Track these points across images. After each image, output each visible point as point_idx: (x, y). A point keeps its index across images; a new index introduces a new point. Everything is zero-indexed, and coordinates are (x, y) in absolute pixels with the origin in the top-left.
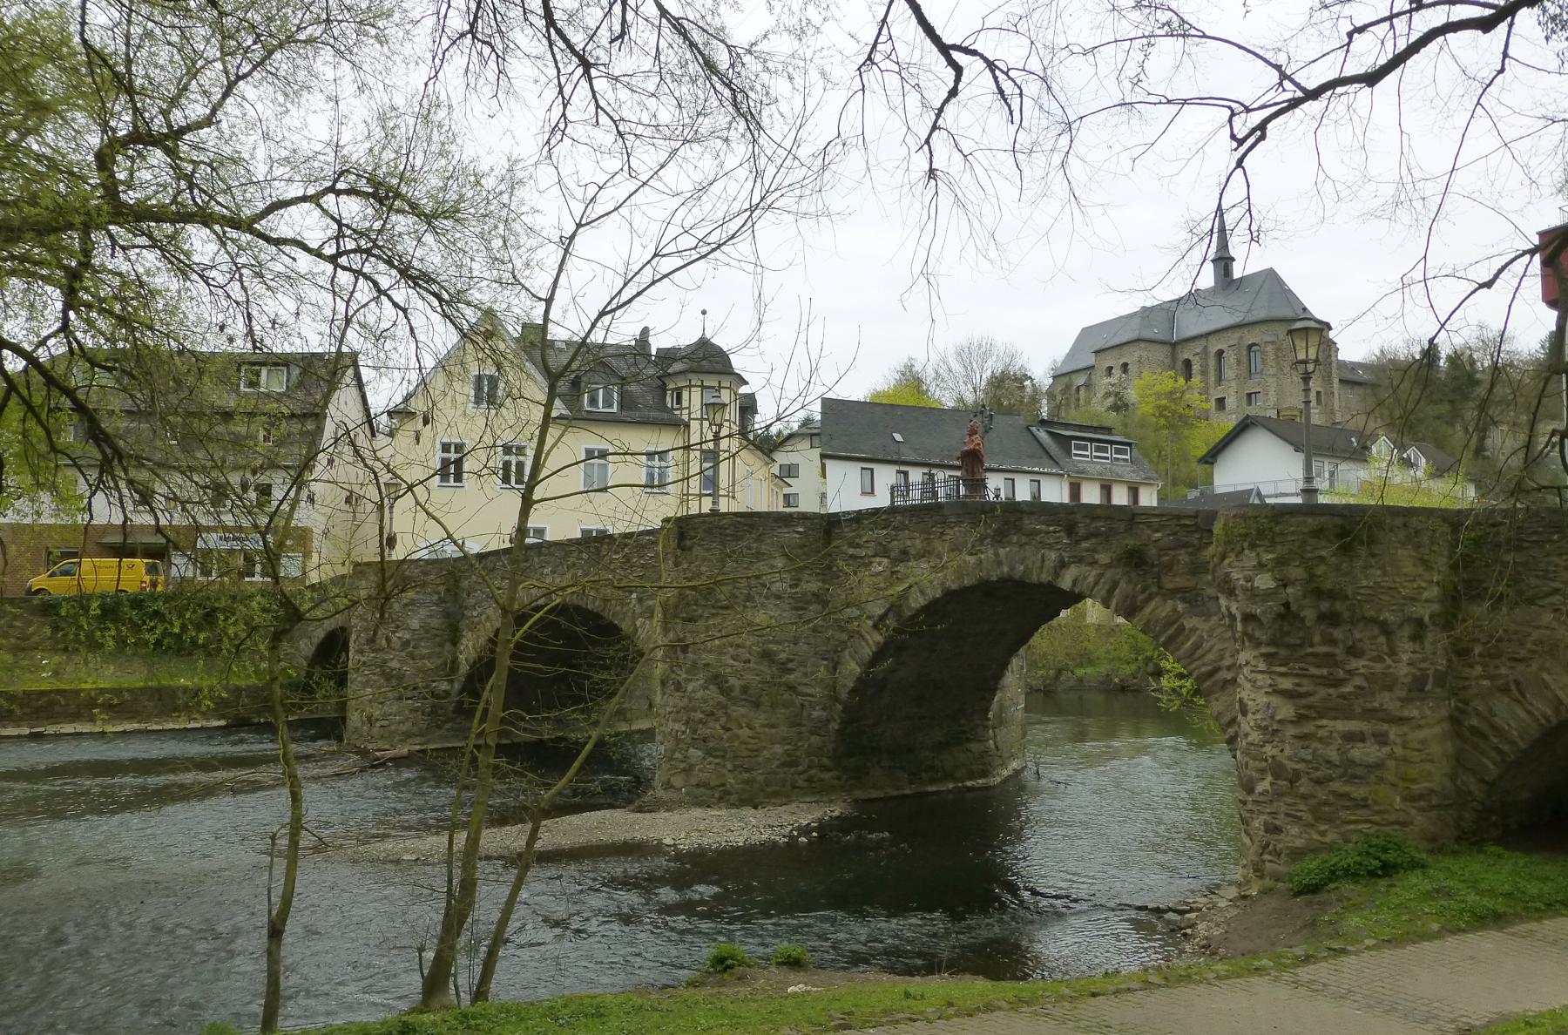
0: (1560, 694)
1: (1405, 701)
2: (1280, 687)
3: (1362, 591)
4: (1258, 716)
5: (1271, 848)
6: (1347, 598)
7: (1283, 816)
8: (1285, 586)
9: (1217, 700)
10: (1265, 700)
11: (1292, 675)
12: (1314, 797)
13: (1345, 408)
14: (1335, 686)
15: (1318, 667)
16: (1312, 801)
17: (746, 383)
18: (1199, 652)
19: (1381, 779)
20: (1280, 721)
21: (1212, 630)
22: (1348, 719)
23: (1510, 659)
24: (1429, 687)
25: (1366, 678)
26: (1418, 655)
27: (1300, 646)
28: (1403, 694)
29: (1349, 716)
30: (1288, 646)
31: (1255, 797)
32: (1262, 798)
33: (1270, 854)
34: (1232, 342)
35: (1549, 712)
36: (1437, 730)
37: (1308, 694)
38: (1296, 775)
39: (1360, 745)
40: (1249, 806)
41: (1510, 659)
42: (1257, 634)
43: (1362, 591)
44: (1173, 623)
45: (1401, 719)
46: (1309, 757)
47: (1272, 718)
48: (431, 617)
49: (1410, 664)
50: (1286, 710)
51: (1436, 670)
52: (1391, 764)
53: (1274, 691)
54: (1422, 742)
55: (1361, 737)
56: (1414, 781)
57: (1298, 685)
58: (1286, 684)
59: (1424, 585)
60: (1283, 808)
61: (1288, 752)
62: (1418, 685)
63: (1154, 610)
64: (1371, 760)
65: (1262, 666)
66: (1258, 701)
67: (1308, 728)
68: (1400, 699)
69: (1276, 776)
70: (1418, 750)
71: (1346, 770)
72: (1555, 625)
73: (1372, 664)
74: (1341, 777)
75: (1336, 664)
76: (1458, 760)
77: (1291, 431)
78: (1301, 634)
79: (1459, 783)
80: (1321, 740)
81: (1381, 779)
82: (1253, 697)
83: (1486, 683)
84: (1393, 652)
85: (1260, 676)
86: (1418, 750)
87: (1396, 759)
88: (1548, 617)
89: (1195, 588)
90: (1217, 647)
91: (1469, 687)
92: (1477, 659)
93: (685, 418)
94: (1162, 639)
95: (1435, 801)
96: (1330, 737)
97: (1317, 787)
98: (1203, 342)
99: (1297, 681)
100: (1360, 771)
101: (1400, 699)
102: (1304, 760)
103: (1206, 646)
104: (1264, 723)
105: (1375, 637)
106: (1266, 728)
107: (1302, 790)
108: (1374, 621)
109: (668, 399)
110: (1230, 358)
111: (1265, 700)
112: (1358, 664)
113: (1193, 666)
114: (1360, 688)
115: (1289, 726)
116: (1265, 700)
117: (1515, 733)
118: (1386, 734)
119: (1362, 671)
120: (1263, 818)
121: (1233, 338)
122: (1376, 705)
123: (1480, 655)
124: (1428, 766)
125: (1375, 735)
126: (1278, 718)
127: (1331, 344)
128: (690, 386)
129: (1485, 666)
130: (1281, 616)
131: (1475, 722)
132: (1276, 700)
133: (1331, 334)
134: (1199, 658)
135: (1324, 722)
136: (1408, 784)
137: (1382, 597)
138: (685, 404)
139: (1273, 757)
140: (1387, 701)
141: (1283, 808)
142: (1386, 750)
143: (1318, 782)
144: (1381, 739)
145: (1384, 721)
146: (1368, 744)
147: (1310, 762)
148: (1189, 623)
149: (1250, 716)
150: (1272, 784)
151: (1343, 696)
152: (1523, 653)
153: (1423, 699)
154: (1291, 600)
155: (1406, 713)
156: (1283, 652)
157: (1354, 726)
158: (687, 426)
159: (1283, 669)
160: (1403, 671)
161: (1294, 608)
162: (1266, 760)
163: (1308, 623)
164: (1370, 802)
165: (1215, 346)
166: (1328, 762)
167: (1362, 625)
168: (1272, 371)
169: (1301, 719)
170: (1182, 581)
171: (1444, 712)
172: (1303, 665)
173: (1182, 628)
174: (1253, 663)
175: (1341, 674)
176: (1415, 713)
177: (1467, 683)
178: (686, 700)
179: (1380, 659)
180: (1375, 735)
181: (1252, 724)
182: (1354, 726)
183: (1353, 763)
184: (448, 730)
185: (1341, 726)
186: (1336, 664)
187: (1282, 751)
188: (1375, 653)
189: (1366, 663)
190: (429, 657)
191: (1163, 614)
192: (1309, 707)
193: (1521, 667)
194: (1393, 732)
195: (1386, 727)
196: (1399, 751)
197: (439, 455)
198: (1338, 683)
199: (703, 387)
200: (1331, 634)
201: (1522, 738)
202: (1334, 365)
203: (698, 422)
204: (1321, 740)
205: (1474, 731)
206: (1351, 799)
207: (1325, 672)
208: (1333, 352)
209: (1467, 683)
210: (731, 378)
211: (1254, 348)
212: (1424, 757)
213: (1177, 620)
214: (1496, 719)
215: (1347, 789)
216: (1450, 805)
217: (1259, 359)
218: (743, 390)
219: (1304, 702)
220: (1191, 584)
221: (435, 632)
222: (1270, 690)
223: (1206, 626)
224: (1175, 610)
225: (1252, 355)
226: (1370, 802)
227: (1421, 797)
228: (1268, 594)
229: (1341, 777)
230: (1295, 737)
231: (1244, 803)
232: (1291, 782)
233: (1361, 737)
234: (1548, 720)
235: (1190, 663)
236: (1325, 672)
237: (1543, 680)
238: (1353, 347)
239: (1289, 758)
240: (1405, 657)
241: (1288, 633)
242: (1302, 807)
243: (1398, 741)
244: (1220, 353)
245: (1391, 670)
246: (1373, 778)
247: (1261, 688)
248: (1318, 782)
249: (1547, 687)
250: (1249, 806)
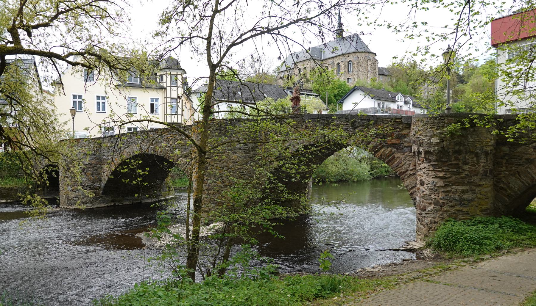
0: (534, 175)
1: (481, 179)
2: (438, 175)
3: (470, 142)
4: (429, 185)
5: (433, 228)
6: (465, 145)
7: (438, 218)
8: (443, 141)
9: (406, 181)
11: (443, 171)
12: (450, 211)
13: (383, 83)
15: (453, 168)
16: (449, 213)
17: (186, 73)
18: (400, 165)
19: (473, 205)
21: (405, 157)
22: (462, 185)
24: (488, 175)
25: (469, 172)
26: (485, 164)
27: (447, 162)
28: (480, 177)
29: (463, 184)
30: (442, 162)
31: (426, 212)
32: (429, 212)
33: (432, 230)
34: (342, 60)
35: (529, 182)
36: (490, 189)
37: (449, 177)
39: (466, 194)
40: (423, 215)
41: (516, 165)
42: (430, 158)
43: (470, 142)
45: (480, 185)
46: (449, 198)
47: (435, 186)
48: (93, 159)
50: (441, 183)
52: (476, 199)
54: (486, 192)
55: (467, 191)
58: (441, 174)
60: (438, 215)
61: (440, 196)
62: (485, 173)
63: (384, 151)
64: (470, 198)
65: (431, 169)
66: (429, 180)
67: (449, 189)
68: (480, 178)
70: (485, 195)
71: (461, 202)
72: (533, 153)
75: (459, 168)
77: (369, 92)
78: (448, 157)
80: (453, 193)
81: (473, 205)
82: (427, 179)
83: (507, 173)
84: (478, 163)
85: (430, 172)
86: (485, 195)
89: (400, 143)
91: (501, 174)
92: (504, 165)
93: (165, 86)
95: (488, 212)
96: (456, 191)
97: (451, 208)
98: (332, 60)
100: (466, 202)
101: (480, 178)
103: (403, 163)
104: (431, 188)
105: (473, 158)
106: (432, 189)
107: (445, 209)
108: (473, 152)
109: (158, 79)
110: (342, 66)
111: (432, 180)
112: (467, 167)
113: (397, 170)
114: (467, 175)
115: (442, 188)
117: (517, 189)
118: (475, 190)
119: (468, 169)
120: (429, 219)
121: (343, 58)
122: (472, 180)
123: (505, 164)
127: (376, 61)
128: (166, 74)
129: (507, 167)
131: (502, 185)
132: (436, 180)
133: (376, 58)
134: (400, 167)
135: (454, 187)
138: (164, 80)
139: (435, 199)
140: (475, 179)
141: (438, 215)
142: (475, 195)
143: (451, 206)
144: (473, 191)
145: (474, 186)
146: (469, 194)
148: (396, 155)
149: (425, 186)
150: (434, 208)
151: (461, 178)
152: (521, 162)
154: (445, 146)
155: (481, 183)
158: (166, 89)
159: (439, 170)
160: (481, 169)
161: (446, 149)
162: (432, 200)
163: (450, 154)
164: (469, 212)
165: (337, 61)
166: (455, 200)
167: (469, 154)
168: (356, 71)
169: (445, 186)
170: (394, 141)
172: (447, 168)
173: (394, 157)
174: (427, 168)
176: (484, 183)
177: (500, 173)
178: (207, 186)
179: (474, 165)
181: (426, 188)
183: (464, 200)
184: (100, 201)
185: (460, 188)
186: (459, 168)
187: (438, 197)
188: (473, 163)
190: (92, 174)
191: (387, 152)
193: (520, 167)
194: (477, 189)
195: (475, 188)
196: (479, 196)
197: (72, 100)
198: (459, 173)
199: (171, 74)
200: (458, 157)
201: (519, 190)
203: (178, 86)
204: (453, 193)
205: (502, 188)
206: (463, 212)
207: (455, 170)
208: (377, 64)
209: (500, 173)
210: (181, 71)
211: (350, 62)
214: (510, 185)
215: (462, 208)
217: (352, 66)
218: (184, 76)
219: (447, 180)
220: (398, 142)
221: (93, 165)
222: (434, 176)
223: (403, 156)
224: (391, 151)
225: (349, 64)
226: (469, 212)
228: (437, 144)
229: (459, 204)
230: (443, 192)
231: (421, 214)
232: (441, 207)
233: (467, 191)
234: (529, 184)
235: (397, 169)
236: (455, 170)
238: (384, 62)
239: (441, 199)
240: (482, 164)
244: (338, 64)
246: (470, 204)
248: (451, 206)
249: (529, 173)
250: (423, 215)
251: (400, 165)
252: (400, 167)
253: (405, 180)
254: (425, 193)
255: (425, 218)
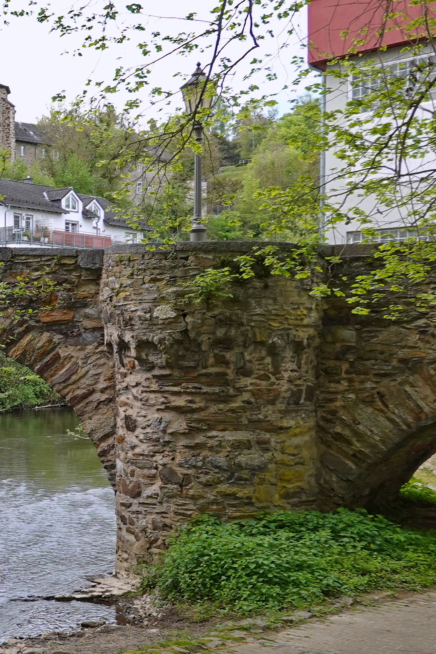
1: (285, 413)
2: (173, 404)
3: (255, 318)
4: (148, 430)
5: (159, 542)
6: (242, 324)
7: (172, 515)
8: (185, 315)
10: (157, 416)
14: (225, 401)
18: (74, 378)
20: (171, 434)
21: (87, 358)
22: (236, 430)
23: (376, 375)
24: (302, 401)
25: (253, 394)
27: (195, 368)
28: (283, 407)
30: (181, 368)
31: (141, 500)
32: (150, 501)
33: (158, 547)
35: (410, 420)
37: (200, 409)
38: (187, 479)
39: (246, 451)
40: (134, 508)
41: (376, 375)
43: (255, 318)
44: (49, 353)
45: (281, 428)
46: (200, 464)
47: (164, 431)
49: (290, 381)
51: (308, 386)
52: (271, 466)
53: (167, 408)
54: (296, 447)
55: (247, 445)
56: (289, 481)
57: (191, 402)
59: (305, 312)
60: (173, 508)
64: (256, 462)
65: (155, 386)
66: (149, 417)
67: (200, 439)
68: (280, 412)
69: (167, 480)
70: (294, 455)
72: (420, 344)
73: (258, 381)
74: (228, 479)
75: (227, 383)
76: (321, 462)
79: (322, 481)
80: (211, 448)
81: (263, 481)
82: (143, 413)
83: (352, 396)
84: (277, 372)
85: (152, 396)
86: (294, 455)
87: (276, 463)
88: (414, 338)
90: (90, 372)
91: (335, 400)
92: (344, 375)
94: (37, 368)
96: (220, 446)
99: (190, 398)
100: (245, 474)
101: (280, 412)
102: (194, 467)
104: (155, 436)
105: (263, 358)
106: (157, 440)
107: (191, 492)
108: (262, 343)
112: (246, 381)
113: (66, 391)
114: (249, 402)
115: (182, 437)
116: (157, 416)
118: (267, 442)
119: (250, 388)
120: (150, 518)
122: (261, 417)
123: (347, 372)
124: (299, 468)
125: (259, 443)
126: (169, 431)
129: (350, 381)
130: (178, 342)
131: (338, 429)
132: (167, 416)
133: (10, 98)
134: (74, 383)
135: (214, 433)
136: (284, 484)
137: (273, 324)
139: (164, 465)
141: (173, 508)
143: (207, 485)
144: (265, 447)
147: (200, 468)
148: (63, 352)
149: (138, 431)
150: (161, 488)
151: (232, 411)
152: (387, 368)
153: (297, 411)
154: (189, 327)
156: (176, 373)
157: (241, 436)
159: (176, 389)
160: (284, 387)
161: (192, 335)
162: (156, 468)
163: (204, 348)
164: (254, 500)
166: (217, 467)
169: (191, 432)
170: (57, 316)
171: (311, 423)
173: (57, 357)
175: (231, 391)
176: (292, 423)
177: (333, 397)
180: (259, 443)
181: (142, 437)
182: (241, 436)
183: (239, 466)
185: (230, 436)
186: (227, 383)
187: (173, 459)
188: (262, 372)
189: (254, 381)
192: (199, 421)
193: (386, 381)
194: (274, 439)
195: (268, 435)
196: (279, 456)
198: (226, 399)
200: (224, 357)
201: (383, 442)
202: (12, 126)
204: (211, 448)
205: (339, 437)
206: (236, 498)
207: (217, 389)
209: (333, 397)
212: (297, 460)
213: (53, 349)
214: (361, 427)
215: (234, 489)
216: (314, 501)
219: (196, 416)
220: (67, 317)
222: (163, 407)
223: (82, 354)
224: (50, 341)
226: (254, 500)
227: (294, 495)
228: (168, 323)
229: (228, 479)
230: (186, 447)
232: (181, 486)
233: (247, 445)
234: (408, 426)
235: (65, 388)
236: (217, 389)
237: (406, 391)
239: (180, 465)
240: (286, 375)
241: (183, 357)
242: (192, 507)
243: (278, 447)
245: (274, 387)
246: (256, 479)
247: (154, 405)
248: (207, 485)
249: (409, 397)
250: (134, 508)
251: (74, 378)
252: (74, 383)
253: (87, 416)
254: (137, 450)
255: (140, 516)
